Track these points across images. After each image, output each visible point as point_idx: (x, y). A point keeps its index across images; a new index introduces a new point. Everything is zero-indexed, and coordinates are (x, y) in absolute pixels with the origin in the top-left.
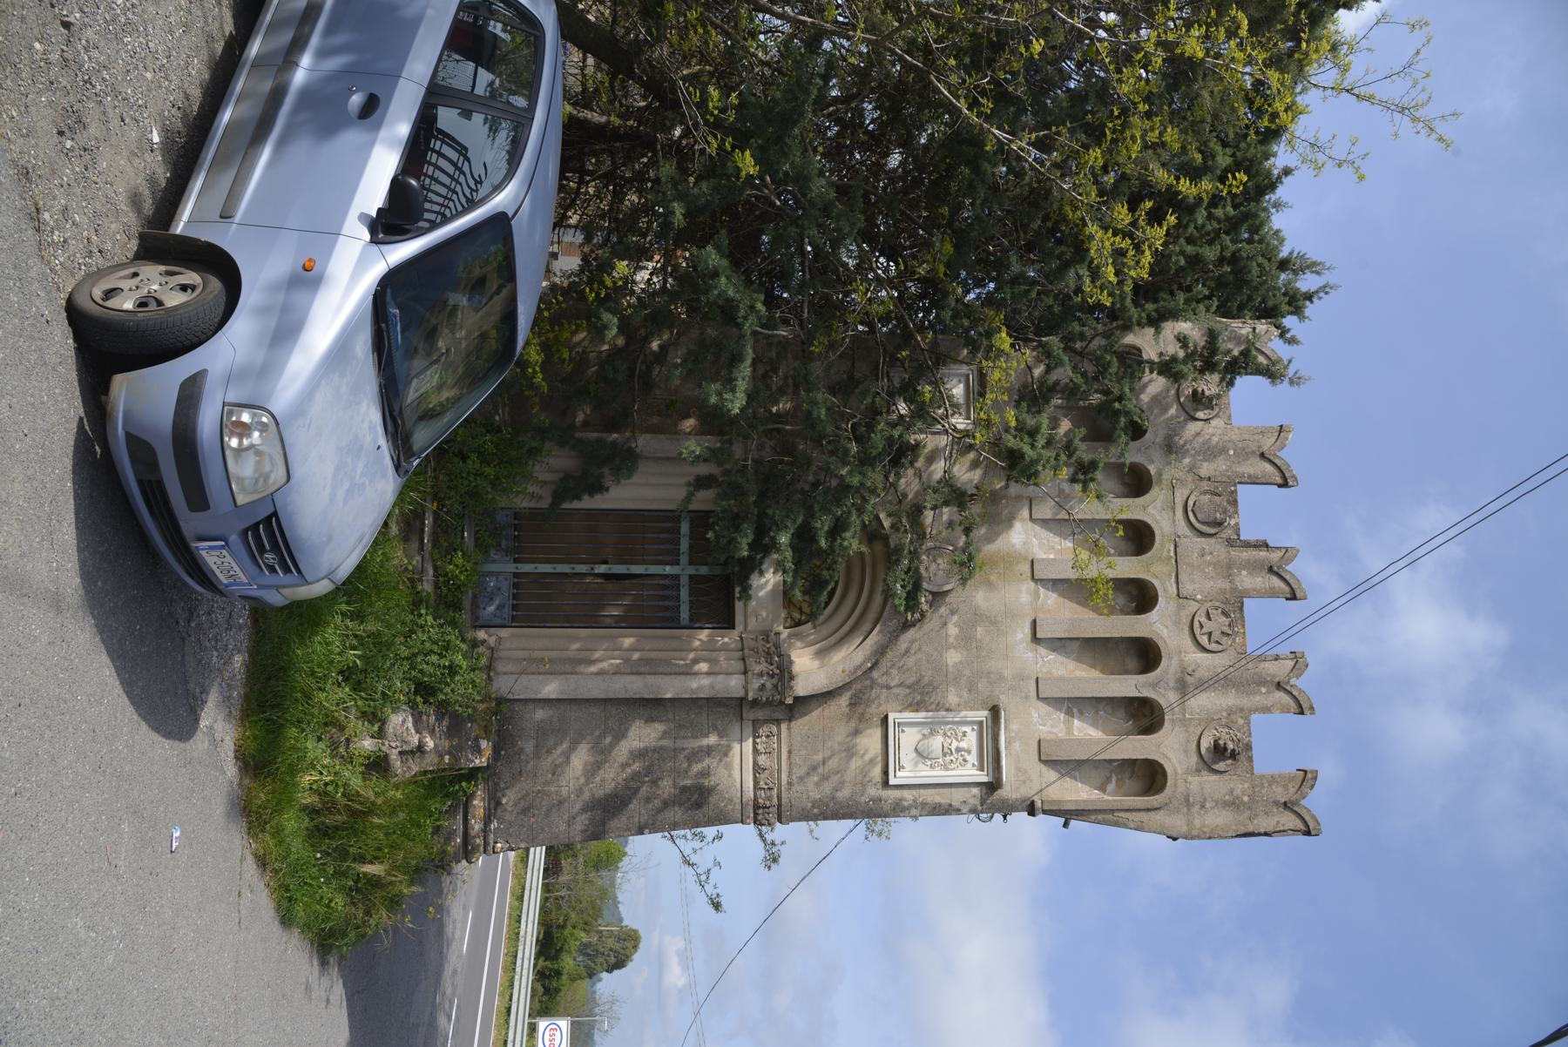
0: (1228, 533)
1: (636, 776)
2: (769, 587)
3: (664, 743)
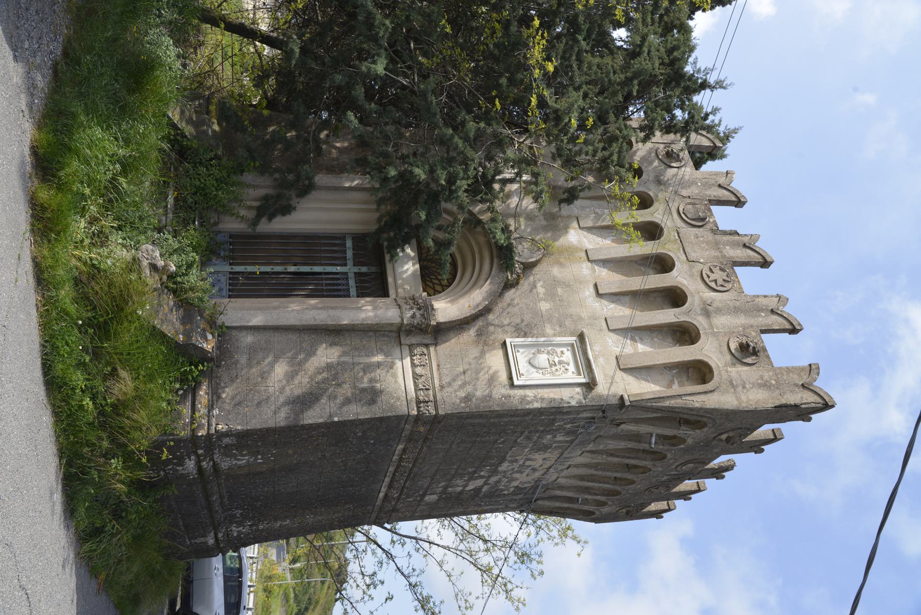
0: (708, 226)
1: (324, 381)
2: (409, 272)
3: (343, 359)
